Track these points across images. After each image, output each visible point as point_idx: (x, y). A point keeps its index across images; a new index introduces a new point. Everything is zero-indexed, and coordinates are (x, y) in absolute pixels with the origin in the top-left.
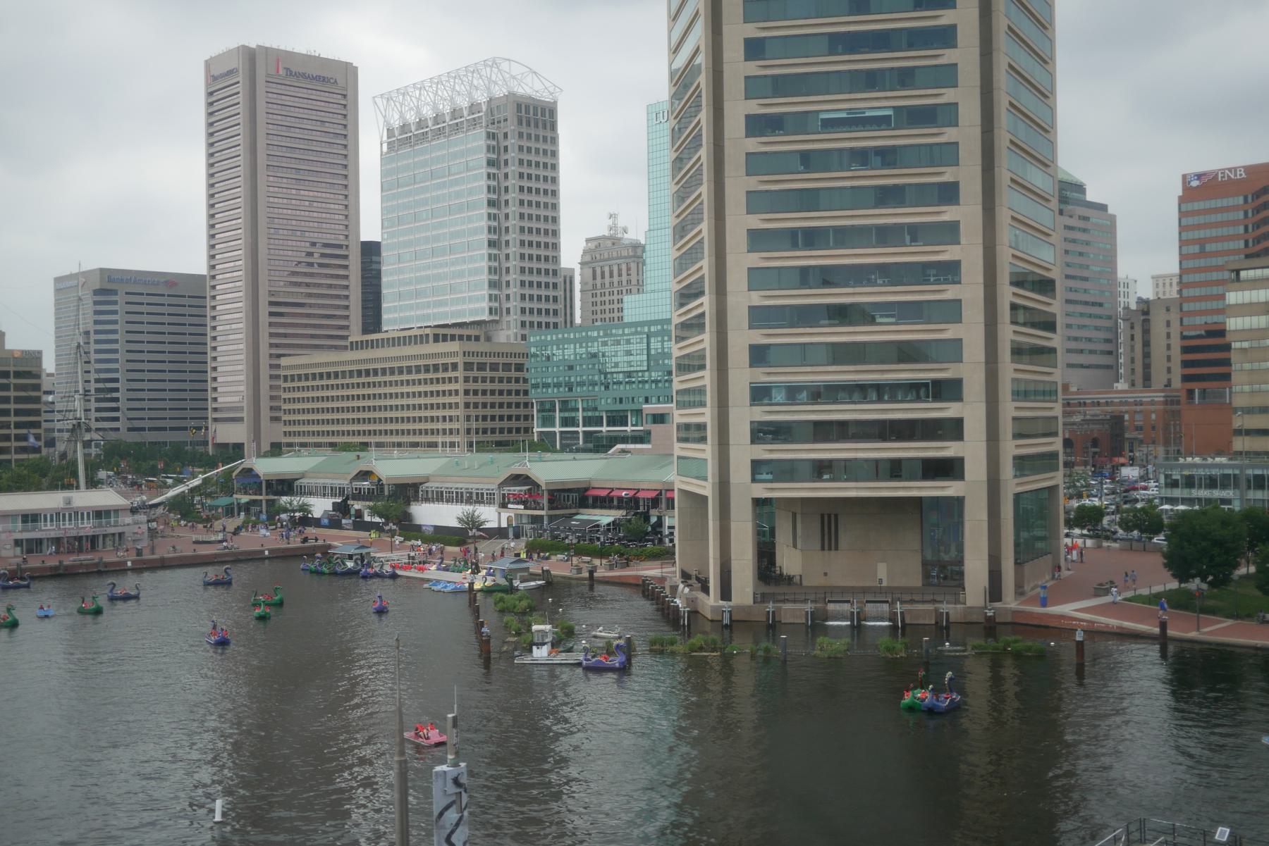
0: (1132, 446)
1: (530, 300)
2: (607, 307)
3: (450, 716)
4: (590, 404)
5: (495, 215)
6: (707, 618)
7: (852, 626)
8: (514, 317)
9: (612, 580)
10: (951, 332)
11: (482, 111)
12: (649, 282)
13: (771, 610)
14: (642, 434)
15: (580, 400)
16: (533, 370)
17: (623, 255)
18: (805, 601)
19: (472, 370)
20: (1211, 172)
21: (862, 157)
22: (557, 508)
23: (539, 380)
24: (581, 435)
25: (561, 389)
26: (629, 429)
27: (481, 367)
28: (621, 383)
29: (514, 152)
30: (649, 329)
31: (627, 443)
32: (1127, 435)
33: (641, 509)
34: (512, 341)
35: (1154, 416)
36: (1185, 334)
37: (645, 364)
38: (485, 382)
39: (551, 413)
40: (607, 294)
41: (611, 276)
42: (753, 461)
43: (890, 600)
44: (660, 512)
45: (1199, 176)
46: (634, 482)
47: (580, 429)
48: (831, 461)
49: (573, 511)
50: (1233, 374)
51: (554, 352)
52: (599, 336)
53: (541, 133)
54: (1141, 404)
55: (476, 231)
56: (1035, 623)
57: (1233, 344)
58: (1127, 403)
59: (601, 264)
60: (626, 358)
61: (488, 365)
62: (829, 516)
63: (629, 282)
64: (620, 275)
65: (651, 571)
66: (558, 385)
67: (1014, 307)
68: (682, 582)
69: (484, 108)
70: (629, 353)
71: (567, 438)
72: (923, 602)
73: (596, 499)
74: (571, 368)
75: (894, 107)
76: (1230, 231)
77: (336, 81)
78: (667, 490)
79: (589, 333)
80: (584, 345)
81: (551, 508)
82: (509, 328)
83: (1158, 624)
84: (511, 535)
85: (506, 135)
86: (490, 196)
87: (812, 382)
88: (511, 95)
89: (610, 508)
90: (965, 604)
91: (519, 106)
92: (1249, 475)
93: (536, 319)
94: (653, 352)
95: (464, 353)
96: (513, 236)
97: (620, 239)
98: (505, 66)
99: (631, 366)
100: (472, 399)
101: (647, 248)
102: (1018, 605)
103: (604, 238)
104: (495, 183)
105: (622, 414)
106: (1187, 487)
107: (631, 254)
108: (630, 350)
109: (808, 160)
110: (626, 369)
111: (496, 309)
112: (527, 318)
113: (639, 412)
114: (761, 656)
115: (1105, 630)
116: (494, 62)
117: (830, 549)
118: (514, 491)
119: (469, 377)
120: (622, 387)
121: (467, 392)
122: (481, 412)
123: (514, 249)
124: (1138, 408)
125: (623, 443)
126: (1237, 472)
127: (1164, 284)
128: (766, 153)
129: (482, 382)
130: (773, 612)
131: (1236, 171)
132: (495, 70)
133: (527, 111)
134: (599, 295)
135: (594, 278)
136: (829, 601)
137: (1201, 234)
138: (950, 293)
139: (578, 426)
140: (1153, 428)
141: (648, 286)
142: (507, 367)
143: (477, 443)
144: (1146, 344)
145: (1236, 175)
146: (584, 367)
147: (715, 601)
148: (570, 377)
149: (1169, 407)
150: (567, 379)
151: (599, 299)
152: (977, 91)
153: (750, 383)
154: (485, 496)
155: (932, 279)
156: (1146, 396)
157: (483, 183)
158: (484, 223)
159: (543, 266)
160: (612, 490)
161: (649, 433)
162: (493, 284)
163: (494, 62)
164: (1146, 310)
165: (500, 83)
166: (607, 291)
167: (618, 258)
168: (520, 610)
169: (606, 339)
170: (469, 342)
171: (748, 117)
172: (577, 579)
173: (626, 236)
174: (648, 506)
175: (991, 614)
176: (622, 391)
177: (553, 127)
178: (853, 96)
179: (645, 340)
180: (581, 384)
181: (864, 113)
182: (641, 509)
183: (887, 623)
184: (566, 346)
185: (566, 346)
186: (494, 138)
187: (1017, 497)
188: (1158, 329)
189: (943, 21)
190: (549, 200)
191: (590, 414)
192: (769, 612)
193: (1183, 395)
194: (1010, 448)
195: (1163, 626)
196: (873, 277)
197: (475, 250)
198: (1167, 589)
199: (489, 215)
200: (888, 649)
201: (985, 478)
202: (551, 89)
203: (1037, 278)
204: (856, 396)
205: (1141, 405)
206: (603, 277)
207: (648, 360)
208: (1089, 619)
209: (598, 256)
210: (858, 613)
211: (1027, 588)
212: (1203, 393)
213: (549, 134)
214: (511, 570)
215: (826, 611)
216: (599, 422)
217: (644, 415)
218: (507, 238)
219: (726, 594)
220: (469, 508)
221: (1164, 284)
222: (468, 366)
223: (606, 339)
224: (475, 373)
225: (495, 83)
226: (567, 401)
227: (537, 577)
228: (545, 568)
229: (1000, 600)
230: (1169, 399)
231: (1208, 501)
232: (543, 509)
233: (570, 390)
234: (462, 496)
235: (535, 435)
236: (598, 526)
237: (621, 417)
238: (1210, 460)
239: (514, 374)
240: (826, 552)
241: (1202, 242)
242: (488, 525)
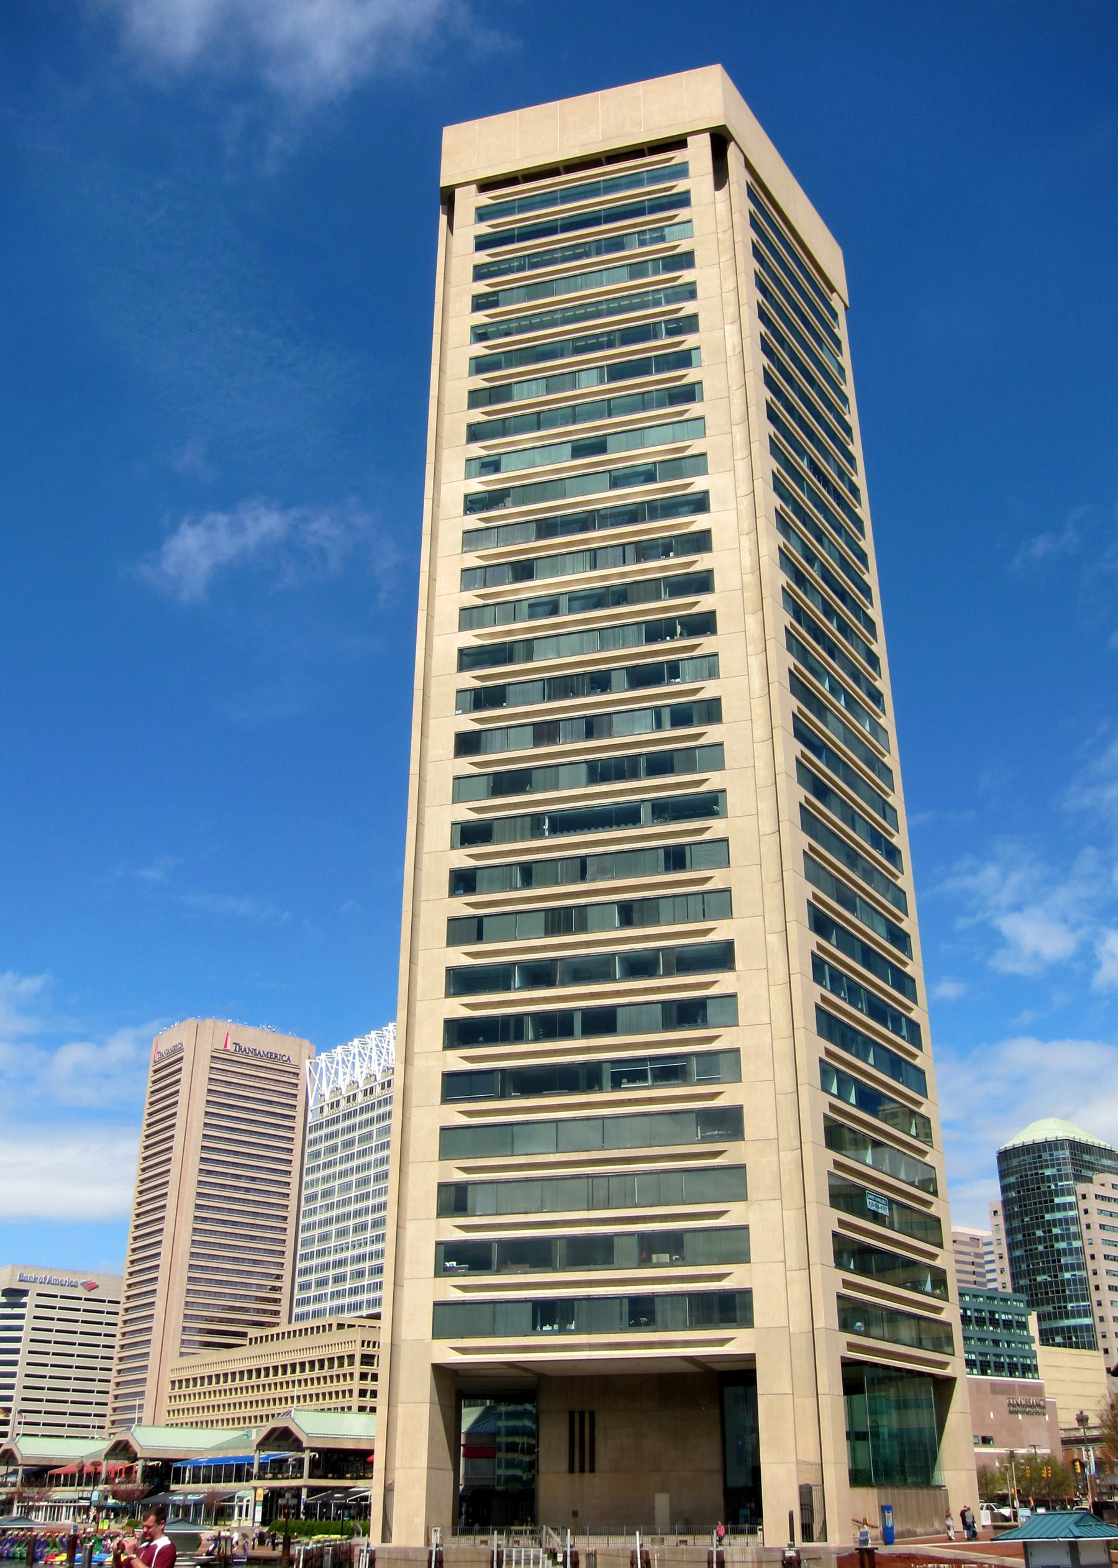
62: (582, 1414)
77: (289, 1059)
95: (363, 1342)
117: (582, 1470)
121: (362, 1393)
171: (451, 921)
208: (952, 1557)
240: (577, 1475)
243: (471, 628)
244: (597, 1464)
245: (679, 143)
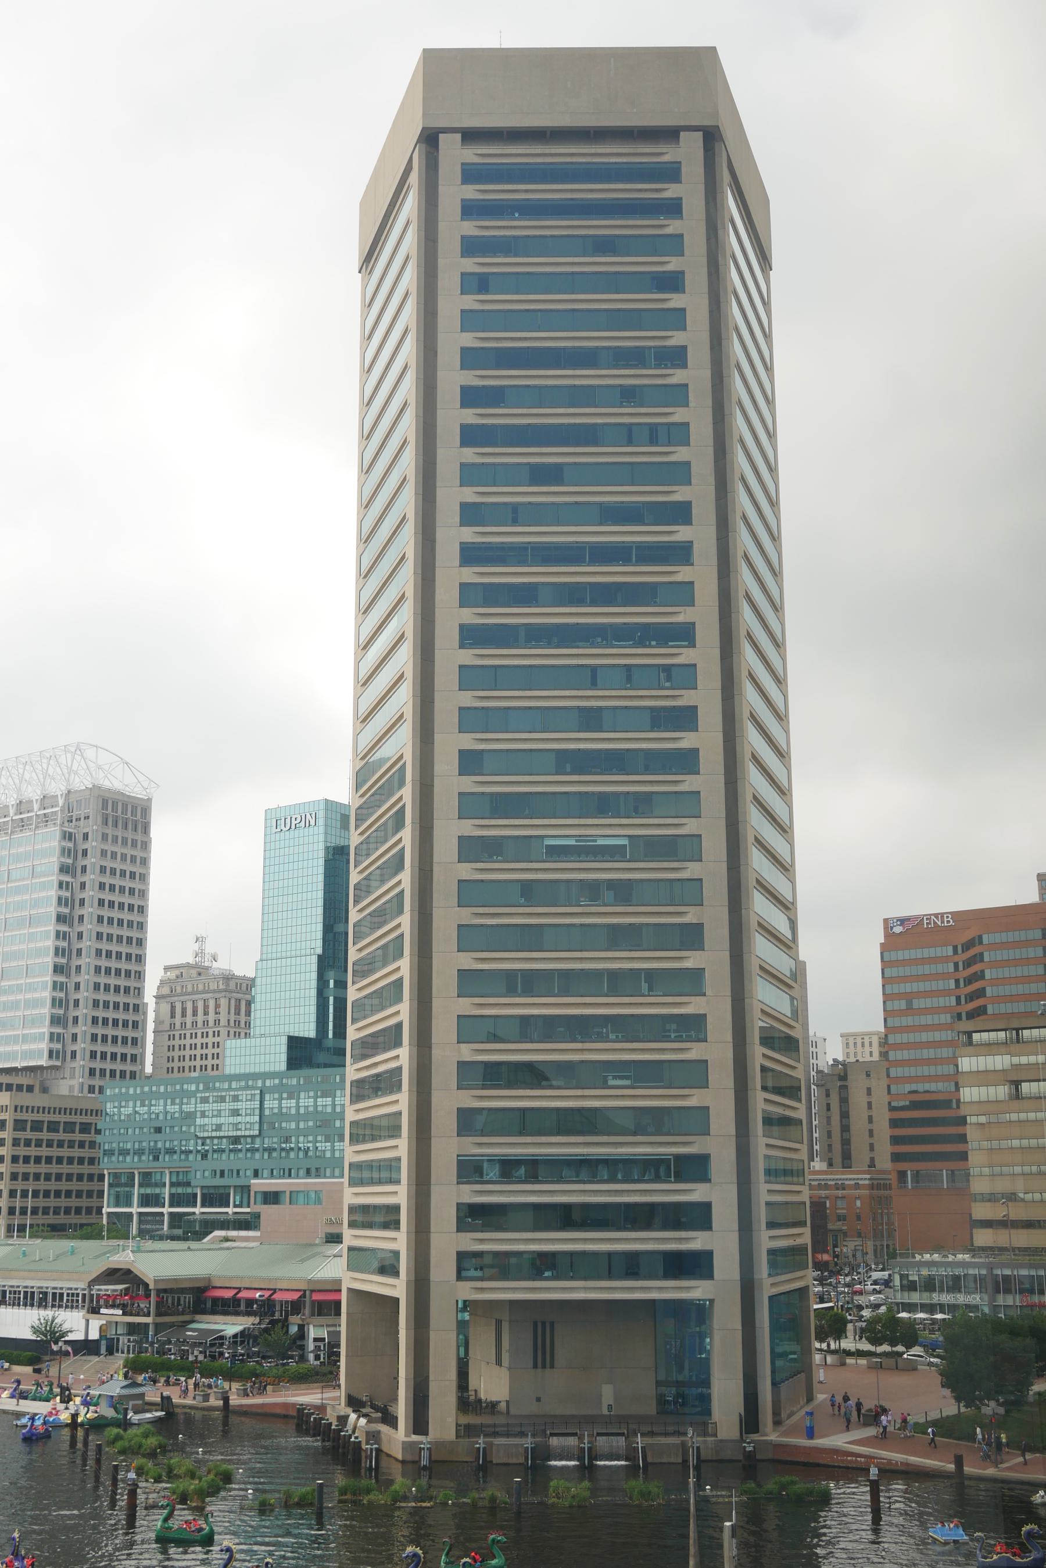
0: (836, 1240)
1: (102, 1041)
2: (187, 1053)
3: (728, 1524)
4: (181, 1177)
5: (65, 933)
6: (396, 1459)
7: (581, 1467)
8: (81, 1063)
9: (254, 1410)
10: (695, 1099)
11: (56, 806)
12: (258, 1024)
13: (482, 1446)
14: (248, 1217)
15: (167, 1172)
16: (168, 1129)
17: (211, 988)
18: (523, 1434)
19: (73, 1132)
20: (916, 917)
21: (592, 891)
22: (165, 1314)
23: (114, 1145)
24: (166, 1217)
25: (144, 1158)
26: (230, 1210)
27: (37, 1126)
28: (223, 1151)
29: (95, 857)
30: (264, 1083)
31: (228, 1229)
32: (830, 1226)
33: (277, 1316)
34: (76, 1094)
35: (858, 1203)
36: (893, 1104)
37: (257, 1126)
38: (40, 1146)
39: (127, 1189)
40: (199, 1035)
41: (195, 1013)
42: (459, 1254)
43: (626, 1432)
44: (303, 1320)
45: (902, 921)
46: (270, 1280)
47: (135, 1210)
48: (554, 1255)
49: (187, 1318)
50: (970, 1153)
51: (137, 1109)
52: (198, 1090)
53: (130, 835)
54: (843, 1187)
55: (39, 952)
56: (802, 1460)
57: (968, 1117)
58: (826, 1187)
59: (182, 998)
60: (231, 1120)
61: (62, 1125)
62: (544, 1324)
63: (217, 1022)
64: (206, 1013)
65: (307, 1397)
66: (139, 1152)
67: (764, 1069)
68: (353, 1411)
69: (61, 802)
70: (235, 1113)
71: (148, 1222)
72: (666, 1434)
73: (215, 1300)
74: (158, 1130)
75: (629, 836)
76: (941, 985)
78: (312, 1291)
79: (185, 1087)
80: (177, 1101)
81: (159, 1314)
82: (73, 1077)
83: (953, 1459)
84: (103, 1349)
85: (86, 837)
86: (60, 909)
87: (533, 1155)
88: (96, 787)
89: (237, 1314)
90: (716, 1435)
91: (105, 802)
92: (997, 1275)
93: (108, 1066)
94: (267, 1112)
95: (16, 1107)
96: (87, 961)
97: (207, 968)
98: (90, 753)
99: (237, 1130)
100: (21, 1168)
101: (258, 982)
102: (778, 1437)
103: (188, 966)
104: (68, 894)
105: (222, 1191)
106: (926, 1291)
107: (221, 987)
108: (238, 1110)
109: (529, 892)
110: (231, 1134)
111: (58, 1052)
112: (98, 1065)
113: (245, 1189)
114: (485, 1507)
115: (888, 1467)
116: (78, 748)
117: (544, 1367)
118: (107, 1290)
119: (19, 1139)
120: (224, 1156)
121: (15, 1159)
122: (42, 1185)
123: (86, 977)
124: (840, 1193)
125: (222, 1229)
126: (984, 1272)
127: (855, 1044)
128: (482, 881)
129: (36, 1146)
130: (484, 1449)
131: (942, 917)
132: (78, 758)
133: (114, 808)
134: (177, 1037)
135: (173, 1016)
136: (552, 1435)
137: (908, 988)
138: (694, 1052)
139: (164, 1206)
140: (859, 1218)
141: (258, 1029)
142: (69, 1127)
143: (31, 1226)
144: (845, 1115)
145: (943, 922)
146: (176, 1129)
147: (406, 1436)
148: (156, 1142)
149: (875, 1192)
150: (152, 1144)
151: (177, 1042)
152: (722, 824)
153: (458, 1156)
154: (65, 1298)
155: (673, 1035)
156: (848, 1178)
157: (53, 893)
158: (50, 943)
159: (121, 999)
160: (239, 1290)
161: (257, 1216)
162: (55, 1020)
163: (78, 748)
164: (842, 1074)
165: (82, 772)
166: (177, 1034)
167: (204, 992)
168: (148, 1451)
169: (207, 1095)
170: (20, 1093)
172: (203, 1409)
173: (215, 965)
174: (287, 1312)
175: (751, 1449)
176: (224, 1161)
177: (146, 829)
178: (583, 821)
179: (258, 1097)
180: (171, 1152)
181: (595, 841)
182: (277, 1316)
183: (623, 1463)
184: (153, 1102)
185: (153, 1102)
186: (70, 839)
187: (771, 1298)
188: (858, 1098)
189: (684, 744)
190: (135, 917)
191: (180, 1190)
192: (479, 1448)
193: (893, 1177)
194: (766, 1240)
195: (959, 1461)
196: (604, 1030)
197: (34, 977)
198: (944, 1415)
199: (58, 933)
200: (642, 1494)
201: (737, 1277)
202: (145, 785)
203: (783, 1035)
204: (584, 1174)
205: (844, 1189)
206: (184, 1014)
207: (261, 1122)
209: (201, 987)
210: (590, 1449)
211: (784, 1415)
212: (917, 1175)
213: (139, 837)
214: (121, 1397)
215: (548, 1447)
216: (191, 1201)
217: (252, 1194)
218: (78, 963)
219: (420, 1424)
220: (48, 1313)
221: (855, 1044)
222: (19, 1125)
223: (207, 1095)
224: (29, 1134)
225: (76, 773)
226: (150, 1173)
227: (154, 1408)
228: (165, 1394)
229: (756, 1431)
230: (875, 1182)
231: (952, 1308)
232: (148, 1315)
233: (156, 1158)
234: (33, 1298)
235: (105, 1216)
236: (222, 1338)
237: (221, 1195)
238: (951, 1258)
239: (77, 1136)
240: (539, 1370)
241: (909, 997)
242: (71, 1337)
243: (471, 646)
244: (556, 1362)
245: (670, 134)
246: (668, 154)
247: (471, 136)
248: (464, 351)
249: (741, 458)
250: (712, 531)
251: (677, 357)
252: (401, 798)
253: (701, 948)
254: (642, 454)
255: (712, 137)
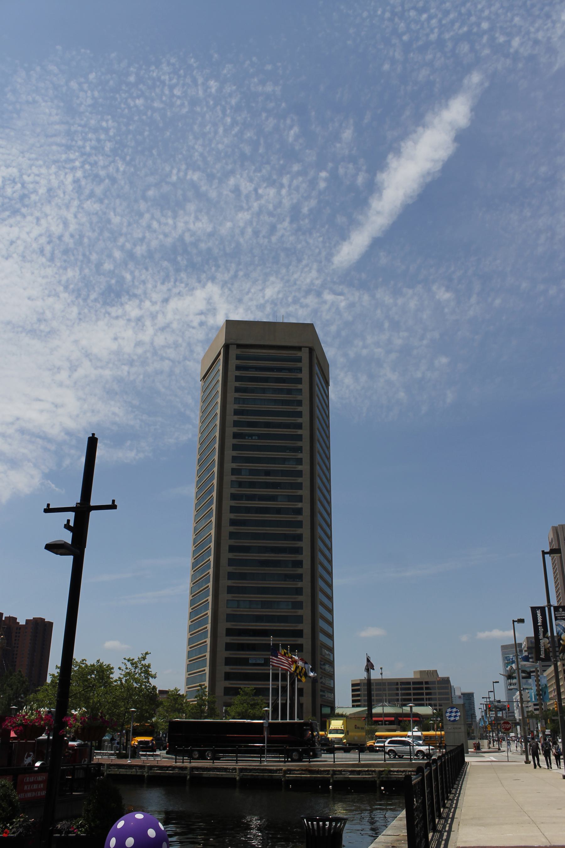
245: (299, 348)
246: (299, 354)
247: (239, 346)
248: (231, 507)
249: (317, 433)
250: (309, 467)
251: (299, 426)
252: (211, 534)
253: (301, 406)
254: (289, 571)
255: (311, 350)
